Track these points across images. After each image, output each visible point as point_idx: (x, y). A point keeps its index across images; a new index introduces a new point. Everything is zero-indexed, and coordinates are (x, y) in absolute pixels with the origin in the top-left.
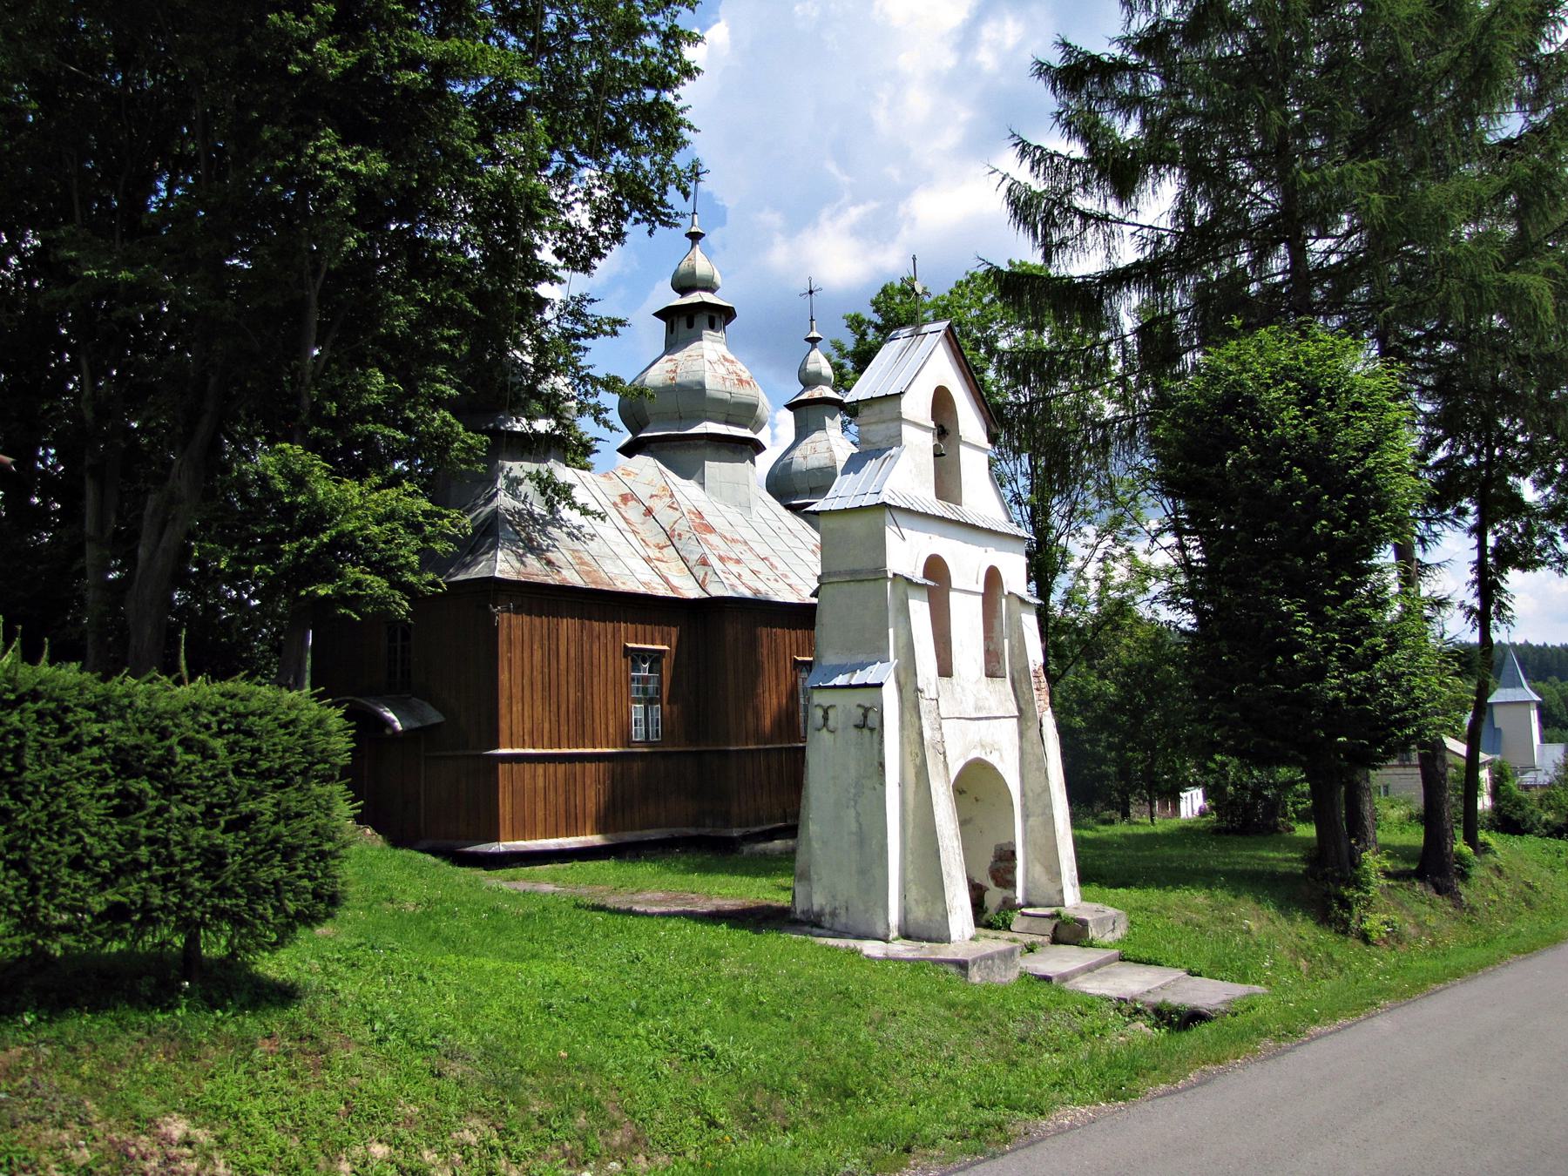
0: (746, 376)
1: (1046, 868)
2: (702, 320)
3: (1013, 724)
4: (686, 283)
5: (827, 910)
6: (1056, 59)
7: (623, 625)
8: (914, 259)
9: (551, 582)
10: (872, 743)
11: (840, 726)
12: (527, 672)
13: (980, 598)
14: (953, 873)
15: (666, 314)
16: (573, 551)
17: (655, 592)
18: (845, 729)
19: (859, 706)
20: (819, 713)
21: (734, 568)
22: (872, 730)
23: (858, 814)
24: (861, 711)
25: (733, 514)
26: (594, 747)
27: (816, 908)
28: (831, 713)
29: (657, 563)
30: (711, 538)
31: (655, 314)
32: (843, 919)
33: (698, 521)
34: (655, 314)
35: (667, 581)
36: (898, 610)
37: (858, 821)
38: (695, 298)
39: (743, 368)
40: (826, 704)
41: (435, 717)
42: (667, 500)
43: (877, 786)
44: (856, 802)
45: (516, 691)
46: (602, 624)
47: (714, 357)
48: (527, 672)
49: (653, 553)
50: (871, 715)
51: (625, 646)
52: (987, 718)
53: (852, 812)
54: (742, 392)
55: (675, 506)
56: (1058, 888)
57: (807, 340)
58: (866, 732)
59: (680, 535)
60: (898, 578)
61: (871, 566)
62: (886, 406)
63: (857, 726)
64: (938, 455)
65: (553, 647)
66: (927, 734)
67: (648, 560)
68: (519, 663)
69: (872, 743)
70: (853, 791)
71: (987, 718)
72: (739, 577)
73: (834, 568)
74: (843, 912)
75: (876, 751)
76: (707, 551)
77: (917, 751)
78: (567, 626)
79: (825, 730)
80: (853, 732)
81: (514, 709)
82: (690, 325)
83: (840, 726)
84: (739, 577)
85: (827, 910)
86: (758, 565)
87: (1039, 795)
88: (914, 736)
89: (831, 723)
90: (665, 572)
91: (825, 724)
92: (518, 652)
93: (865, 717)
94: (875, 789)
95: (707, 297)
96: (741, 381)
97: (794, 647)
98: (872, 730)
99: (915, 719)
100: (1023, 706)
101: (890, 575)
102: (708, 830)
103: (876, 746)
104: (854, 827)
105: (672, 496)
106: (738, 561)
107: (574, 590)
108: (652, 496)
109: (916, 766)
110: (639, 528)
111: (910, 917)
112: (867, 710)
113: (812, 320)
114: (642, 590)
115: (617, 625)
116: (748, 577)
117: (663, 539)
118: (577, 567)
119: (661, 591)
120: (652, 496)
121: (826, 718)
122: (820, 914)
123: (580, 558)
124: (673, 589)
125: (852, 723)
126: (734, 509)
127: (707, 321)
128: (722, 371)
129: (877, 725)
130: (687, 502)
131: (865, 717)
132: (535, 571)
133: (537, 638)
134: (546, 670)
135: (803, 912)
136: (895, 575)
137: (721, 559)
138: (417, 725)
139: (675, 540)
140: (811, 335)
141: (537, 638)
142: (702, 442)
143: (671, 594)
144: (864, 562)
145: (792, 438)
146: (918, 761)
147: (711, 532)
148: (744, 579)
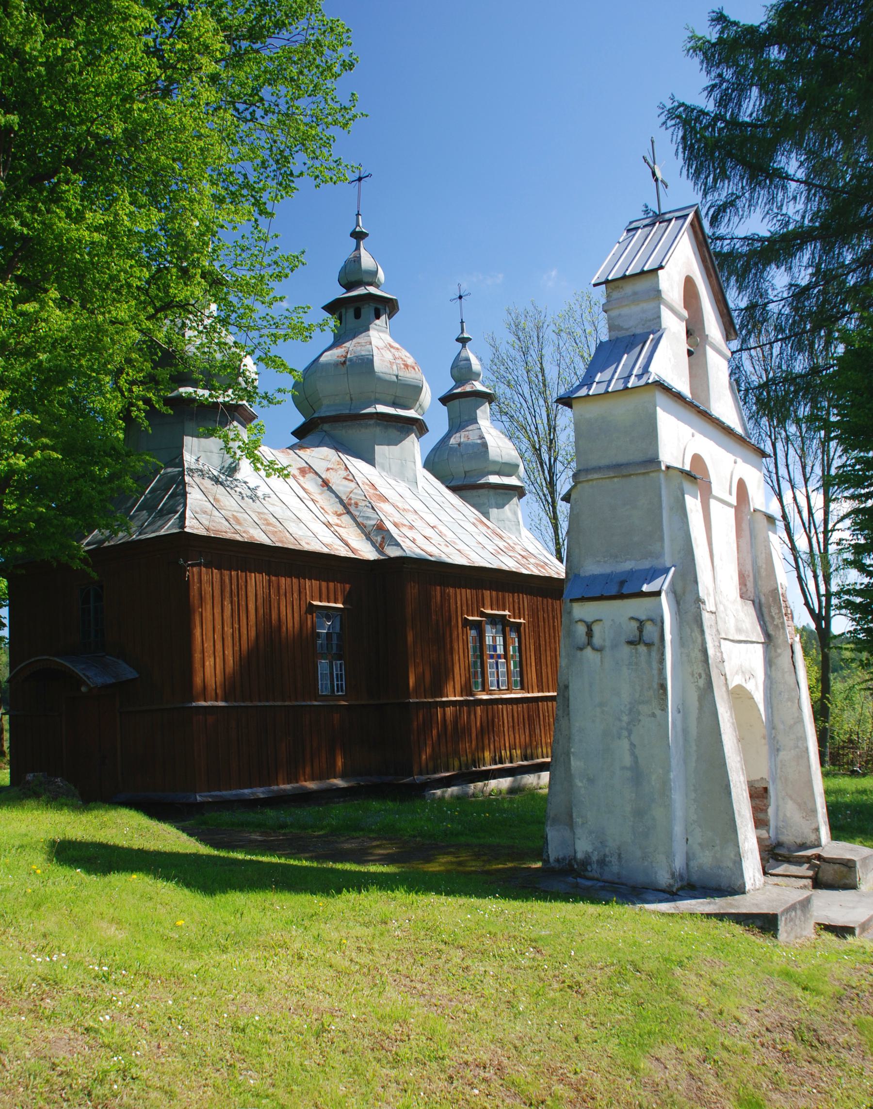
0: (410, 361)
1: (799, 805)
2: (367, 310)
3: (759, 649)
4: (353, 278)
5: (595, 858)
6: (712, 34)
7: (308, 582)
8: (653, 142)
9: (240, 539)
10: (649, 663)
11: (608, 644)
12: (218, 627)
13: (733, 510)
14: (743, 813)
15: (332, 307)
16: (259, 513)
17: (337, 553)
18: (614, 646)
19: (632, 618)
20: (581, 629)
21: (410, 534)
22: (649, 645)
23: (633, 745)
24: (635, 624)
25: (402, 487)
26: (284, 701)
27: (580, 856)
28: (596, 628)
29: (337, 528)
30: (386, 507)
31: (323, 308)
32: (615, 869)
33: (372, 491)
34: (323, 308)
35: (347, 545)
36: (671, 509)
37: (633, 754)
38: (361, 291)
39: (408, 355)
40: (589, 619)
41: (130, 673)
42: (344, 473)
43: (658, 712)
44: (630, 732)
45: (208, 645)
46: (289, 580)
47: (381, 344)
48: (218, 627)
49: (333, 519)
50: (649, 627)
51: (310, 603)
52: (746, 642)
53: (625, 744)
54: (408, 375)
55: (351, 477)
56: (814, 826)
57: (458, 340)
58: (642, 648)
59: (356, 504)
60: (671, 471)
61: (638, 457)
62: (641, 285)
63: (630, 643)
64: (690, 353)
65: (243, 603)
66: (711, 652)
67: (328, 525)
68: (210, 617)
69: (649, 663)
70: (625, 718)
71: (746, 642)
72: (414, 541)
73: (595, 460)
74: (614, 860)
75: (655, 672)
76: (383, 518)
77: (701, 671)
78: (256, 582)
79: (589, 649)
80: (626, 649)
81: (207, 663)
82: (358, 315)
83: (608, 644)
84: (414, 541)
85: (595, 858)
86: (429, 532)
87: (791, 727)
88: (697, 654)
89: (597, 640)
90: (345, 536)
91: (590, 643)
92: (209, 607)
93: (641, 629)
94: (654, 715)
95: (372, 290)
96: (406, 366)
97: (465, 608)
98: (649, 645)
99: (696, 634)
100: (772, 632)
101: (663, 468)
102: (580, 784)
103: (655, 665)
104: (628, 761)
105: (347, 468)
106: (412, 527)
107: (261, 547)
108: (328, 469)
109: (698, 688)
110: (317, 497)
111: (692, 864)
112: (641, 624)
113: (462, 322)
114: (325, 550)
115: (302, 581)
116: (420, 541)
117: (340, 509)
118: (263, 527)
119: (343, 552)
120: (328, 469)
121: (590, 633)
122: (586, 863)
123: (266, 520)
124: (353, 550)
125: (623, 638)
126: (403, 484)
127: (372, 312)
128: (388, 356)
129: (656, 640)
130: (361, 475)
131: (641, 629)
132: (224, 529)
133: (227, 595)
134: (236, 626)
135: (558, 860)
136: (668, 467)
137: (396, 525)
138: (110, 680)
139: (352, 509)
140: (461, 336)
141: (227, 595)
142: (372, 422)
143: (353, 556)
144: (634, 454)
145: (445, 429)
146: (701, 682)
147: (384, 501)
148: (417, 542)
